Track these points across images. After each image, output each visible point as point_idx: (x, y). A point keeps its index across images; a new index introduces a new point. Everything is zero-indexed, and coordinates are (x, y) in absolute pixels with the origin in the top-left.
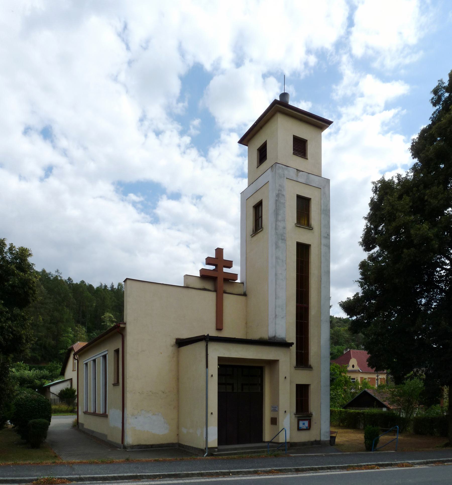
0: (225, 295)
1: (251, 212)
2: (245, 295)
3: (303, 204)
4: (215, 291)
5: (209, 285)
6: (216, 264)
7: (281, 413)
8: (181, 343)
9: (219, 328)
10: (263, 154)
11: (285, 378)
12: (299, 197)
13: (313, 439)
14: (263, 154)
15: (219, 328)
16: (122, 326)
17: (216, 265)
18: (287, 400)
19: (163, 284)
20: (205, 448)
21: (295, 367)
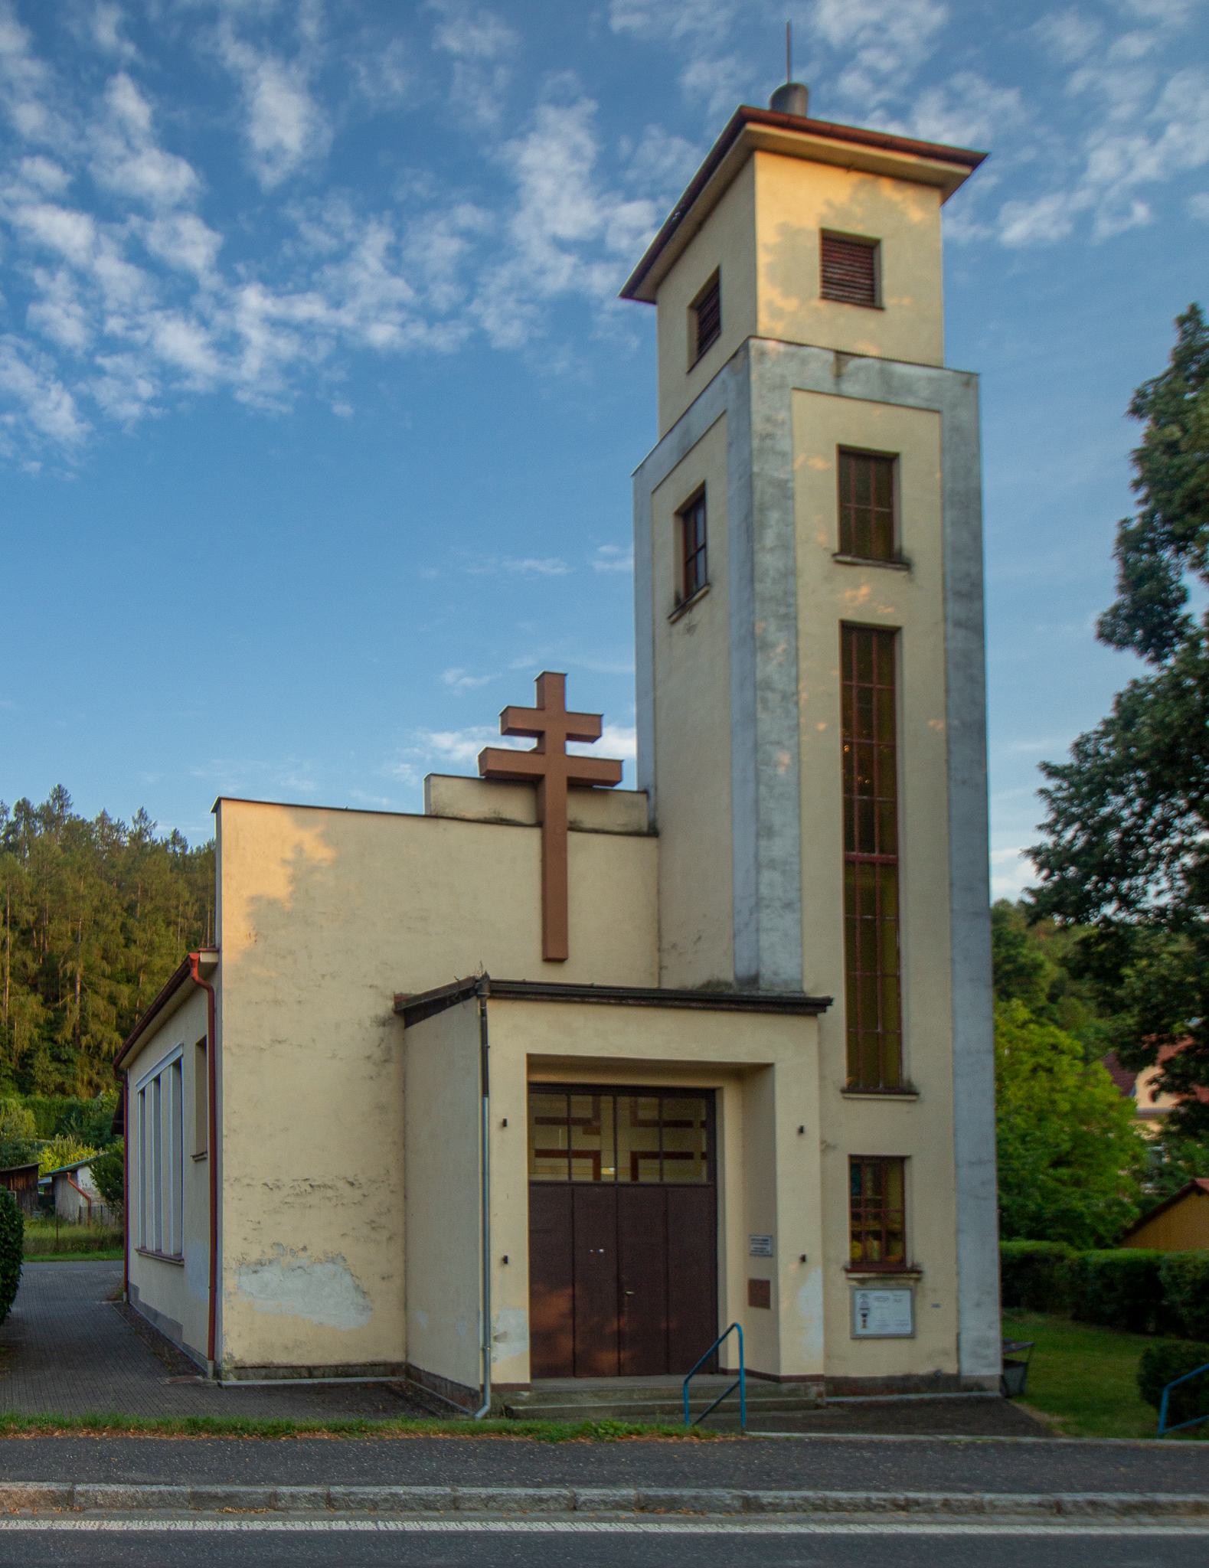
0: (573, 838)
1: (668, 532)
2: (652, 832)
4: (539, 824)
5: (516, 804)
6: (540, 728)
7: (786, 1266)
8: (412, 1011)
9: (554, 956)
11: (801, 1130)
13: (924, 1369)
15: (551, 955)
16: (205, 958)
17: (539, 735)
18: (807, 1211)
19: (346, 810)
20: (483, 1387)
21: (843, 1091)
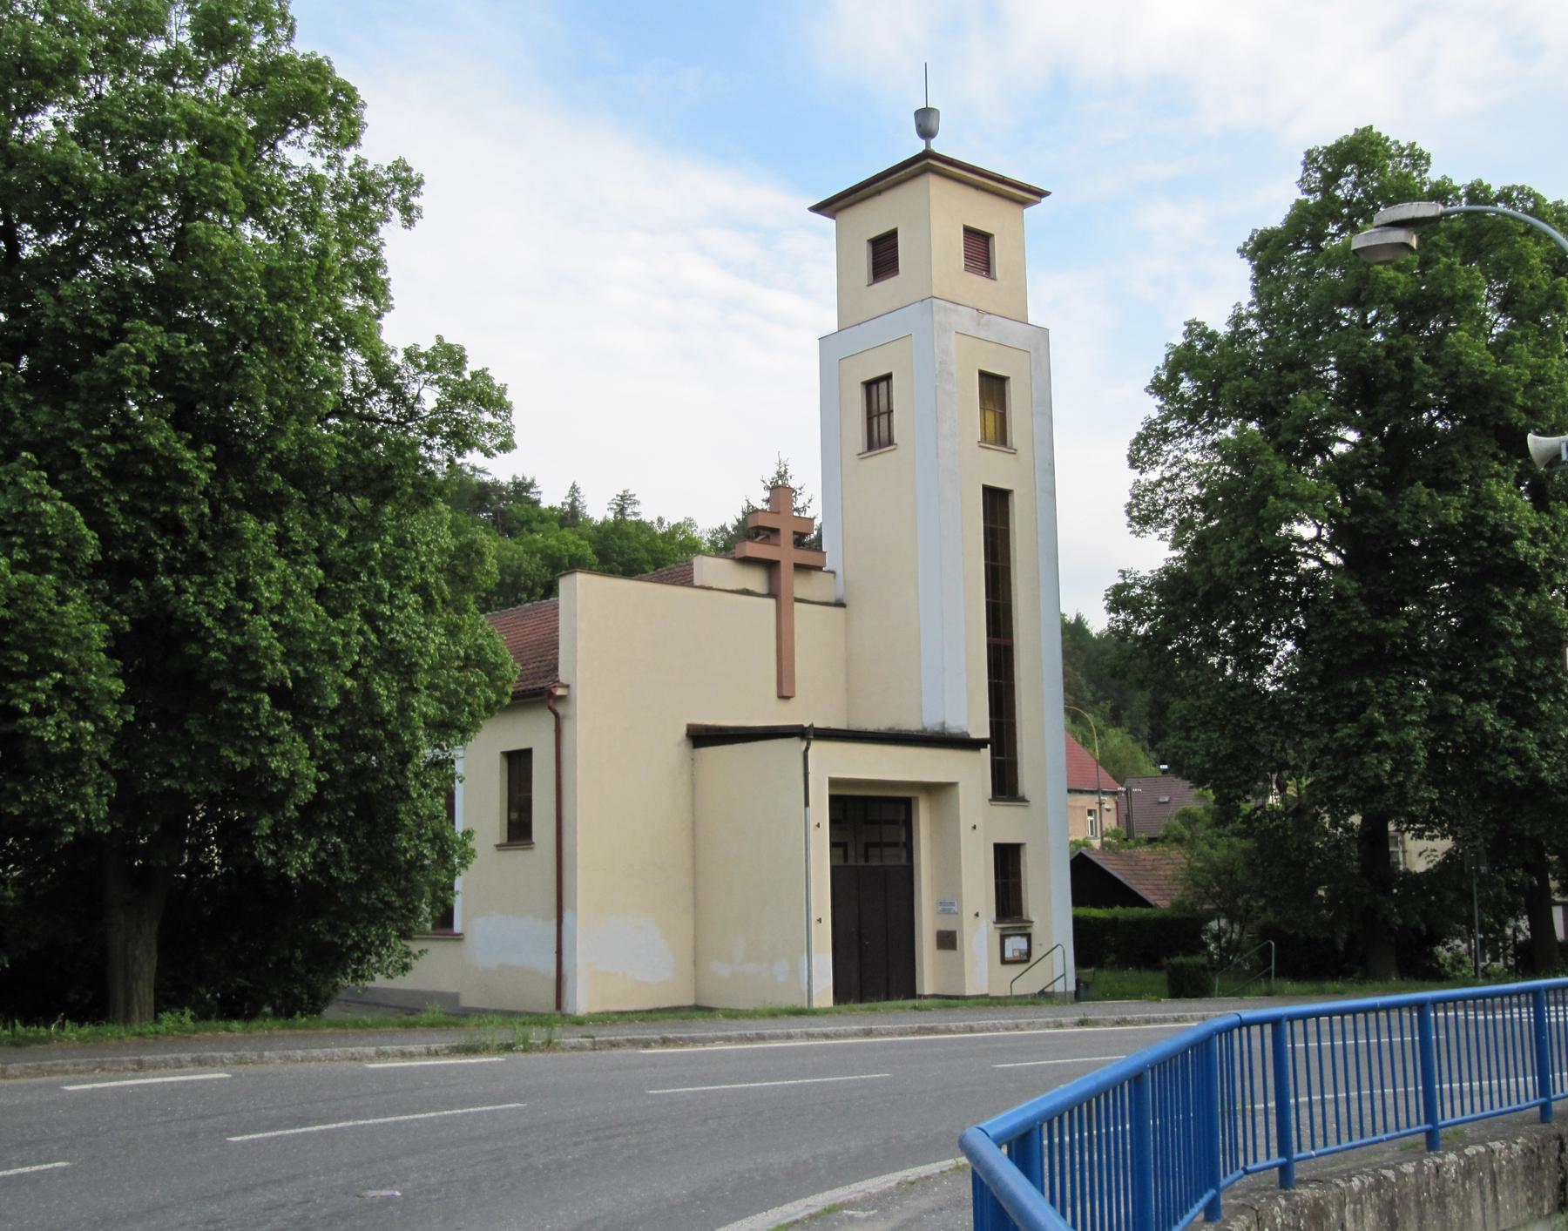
2: (840, 604)
3: (993, 387)
4: (773, 593)
8: (702, 737)
10: (884, 256)
12: (983, 375)
14: (884, 256)
